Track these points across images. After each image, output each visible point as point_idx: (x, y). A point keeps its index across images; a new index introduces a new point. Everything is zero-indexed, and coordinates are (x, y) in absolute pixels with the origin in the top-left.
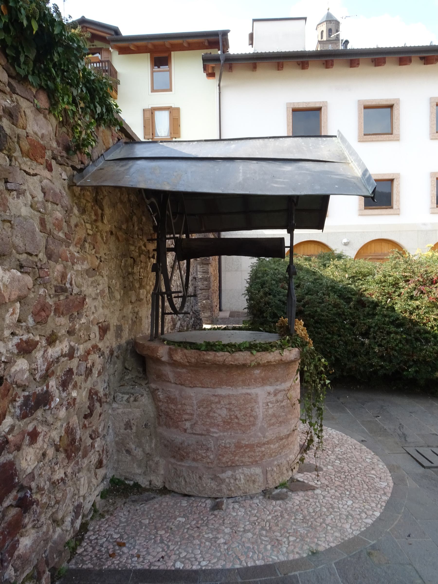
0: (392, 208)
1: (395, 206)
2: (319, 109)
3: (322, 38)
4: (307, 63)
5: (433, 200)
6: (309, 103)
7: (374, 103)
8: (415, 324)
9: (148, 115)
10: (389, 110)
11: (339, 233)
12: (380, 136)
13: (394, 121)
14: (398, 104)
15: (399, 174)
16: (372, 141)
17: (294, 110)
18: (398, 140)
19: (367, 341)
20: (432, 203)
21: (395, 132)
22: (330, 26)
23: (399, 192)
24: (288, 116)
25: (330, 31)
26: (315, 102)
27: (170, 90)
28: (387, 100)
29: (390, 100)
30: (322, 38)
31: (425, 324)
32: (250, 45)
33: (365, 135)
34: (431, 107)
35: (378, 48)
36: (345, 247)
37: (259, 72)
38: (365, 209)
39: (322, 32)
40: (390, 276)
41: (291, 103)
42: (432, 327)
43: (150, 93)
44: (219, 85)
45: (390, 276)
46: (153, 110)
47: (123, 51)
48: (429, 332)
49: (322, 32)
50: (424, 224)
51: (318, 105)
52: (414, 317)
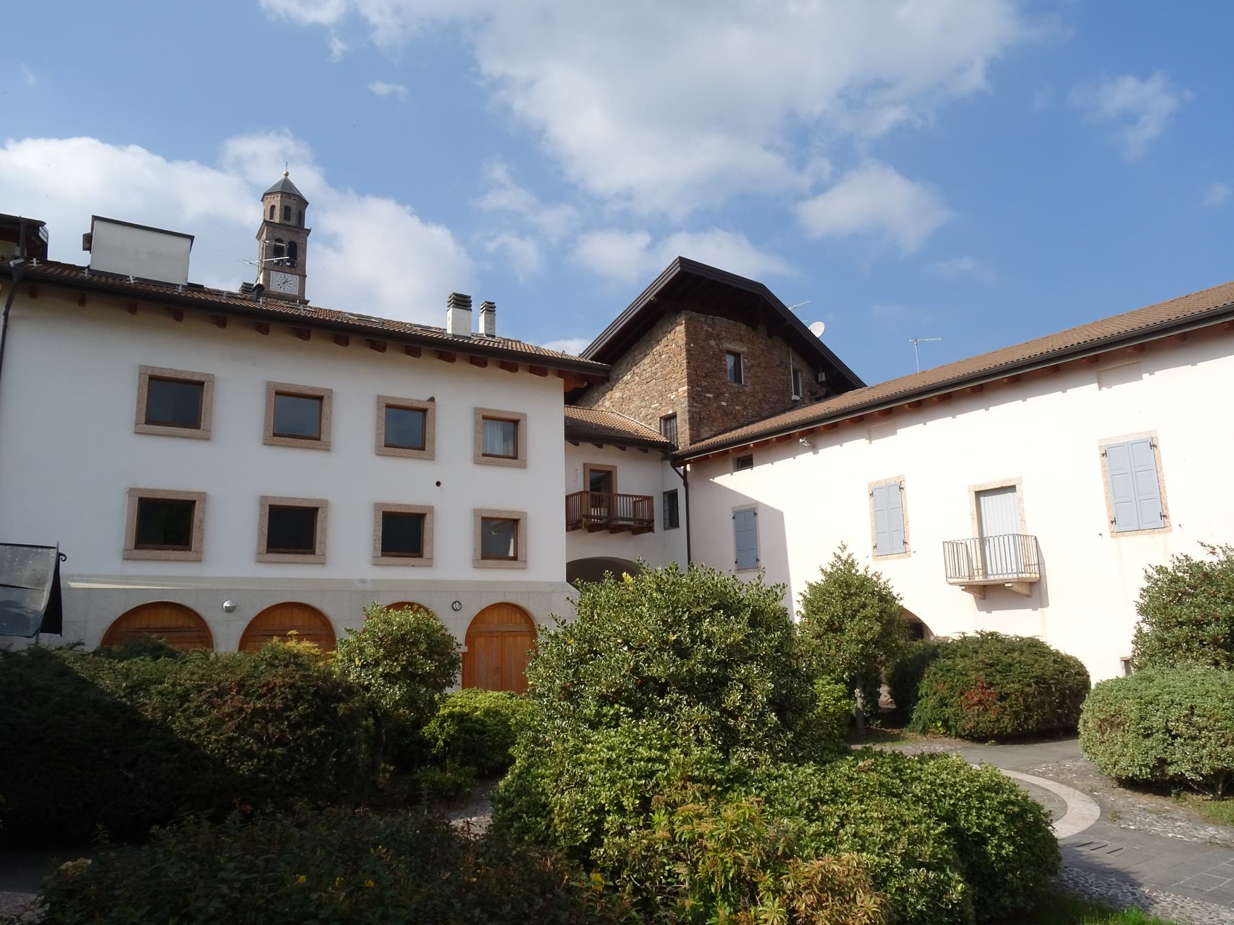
0: (313, 553)
1: (318, 551)
2: (202, 384)
3: (272, 216)
6: (181, 372)
7: (293, 390)
8: (192, 746)
10: (318, 402)
13: (323, 421)
14: (330, 397)
15: (326, 501)
17: (153, 378)
19: (131, 775)
21: (323, 437)
22: (289, 202)
23: (325, 529)
25: (287, 211)
26: (194, 373)
28: (312, 389)
29: (318, 389)
30: (272, 216)
31: (205, 747)
32: (85, 249)
33: (275, 435)
34: (379, 408)
38: (268, 552)
39: (273, 207)
40: (180, 685)
41: (148, 367)
42: (212, 751)
44: (6, 314)
45: (180, 685)
48: (207, 757)
49: (273, 207)
50: (363, 581)
51: (197, 378)
52: (193, 739)
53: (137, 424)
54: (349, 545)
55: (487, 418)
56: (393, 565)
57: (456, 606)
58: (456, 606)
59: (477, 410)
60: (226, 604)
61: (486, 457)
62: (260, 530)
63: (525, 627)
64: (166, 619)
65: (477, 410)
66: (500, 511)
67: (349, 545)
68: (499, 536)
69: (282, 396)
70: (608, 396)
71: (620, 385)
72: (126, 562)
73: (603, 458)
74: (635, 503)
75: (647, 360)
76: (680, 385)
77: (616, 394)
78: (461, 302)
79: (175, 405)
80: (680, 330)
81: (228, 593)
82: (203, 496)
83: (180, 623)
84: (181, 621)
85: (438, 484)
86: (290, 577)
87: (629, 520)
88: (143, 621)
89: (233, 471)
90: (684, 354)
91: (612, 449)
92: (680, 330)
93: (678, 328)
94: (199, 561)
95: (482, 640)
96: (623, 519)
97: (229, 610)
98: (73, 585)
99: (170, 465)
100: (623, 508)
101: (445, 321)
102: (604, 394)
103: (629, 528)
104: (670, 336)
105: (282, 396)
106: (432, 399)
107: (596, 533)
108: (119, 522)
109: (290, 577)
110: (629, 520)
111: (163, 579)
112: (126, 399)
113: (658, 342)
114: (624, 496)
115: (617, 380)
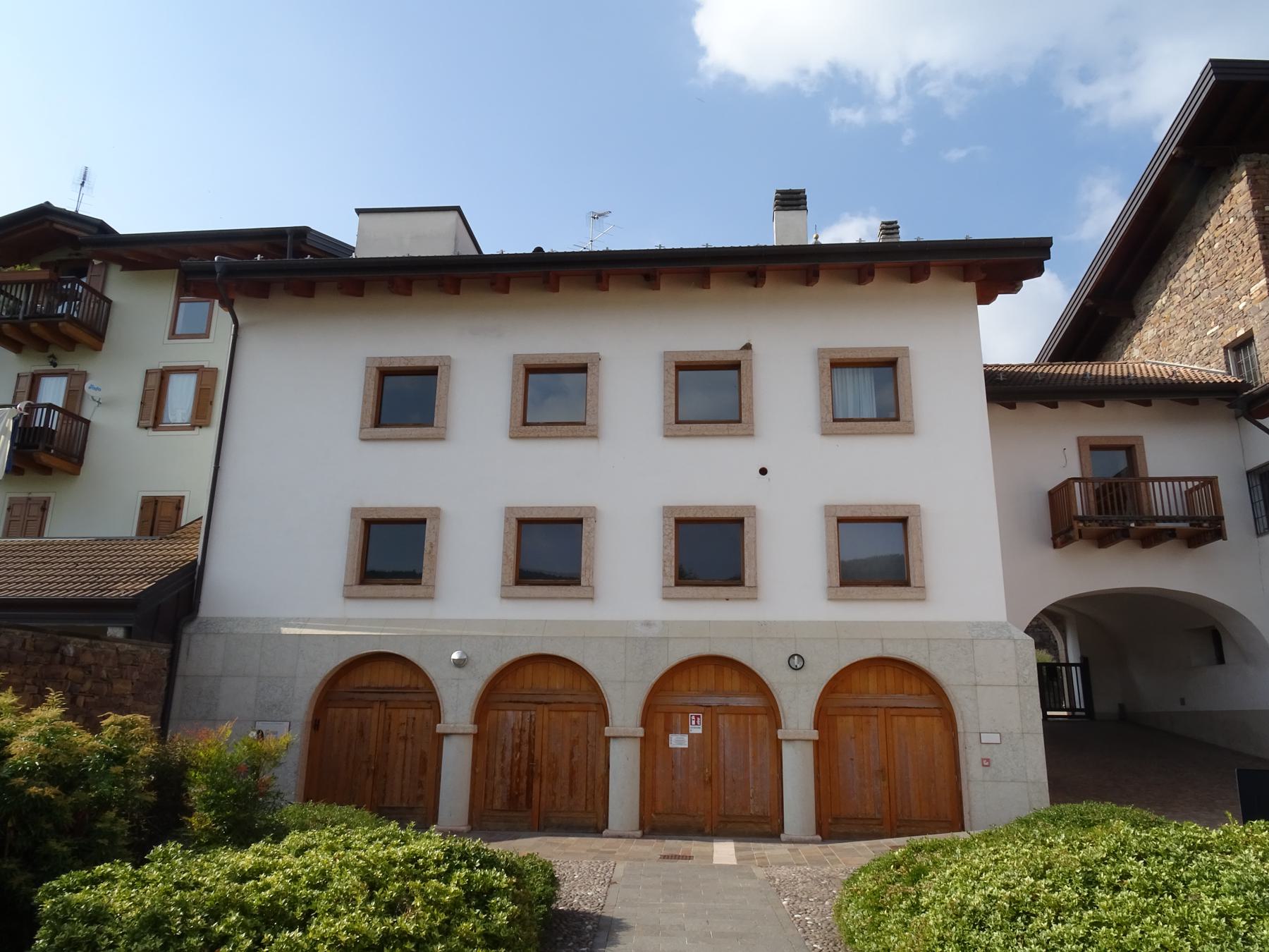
4: (816, 275)
5: (667, 569)
6: (412, 358)
9: (154, 381)
11: (473, 636)
12: (554, 428)
15: (593, 509)
16: (538, 437)
18: (595, 437)
20: (665, 575)
23: (592, 549)
24: (366, 383)
27: (207, 336)
28: (571, 356)
29: (579, 355)
35: (502, 255)
36: (457, 670)
37: (822, 287)
43: (167, 341)
46: (164, 376)
47: (130, 265)
50: (648, 624)
51: (429, 364)
53: (361, 428)
54: (470, 561)
55: (840, 364)
56: (714, 599)
57: (796, 663)
58: (796, 663)
59: (821, 353)
60: (455, 656)
61: (838, 421)
62: (505, 554)
63: (927, 702)
64: (387, 676)
65: (821, 353)
66: (870, 507)
67: (470, 561)
68: (877, 554)
69: (533, 370)
70: (1136, 341)
71: (1153, 318)
72: (504, 601)
73: (1112, 424)
74: (1189, 492)
75: (1191, 262)
76: (1252, 282)
77: (1148, 333)
78: (791, 200)
79: (404, 401)
80: (1240, 194)
81: (457, 641)
82: (436, 512)
83: (406, 682)
84: (407, 679)
85: (763, 471)
86: (709, 620)
87: (1184, 519)
88: (366, 678)
89: (474, 476)
90: (1253, 227)
91: (1132, 409)
92: (1240, 194)
93: (1235, 190)
94: (430, 597)
95: (851, 719)
96: (1158, 519)
97: (459, 664)
98: (285, 631)
99: (399, 475)
100: (1164, 501)
101: (767, 230)
102: (1130, 340)
103: (1172, 534)
104: (1223, 208)
105: (533, 370)
106: (748, 347)
107: (1113, 549)
108: (335, 551)
109: (709, 620)
110: (1184, 519)
111: (388, 621)
112: (349, 394)
113: (1204, 227)
114: (1159, 480)
115: (1147, 312)
